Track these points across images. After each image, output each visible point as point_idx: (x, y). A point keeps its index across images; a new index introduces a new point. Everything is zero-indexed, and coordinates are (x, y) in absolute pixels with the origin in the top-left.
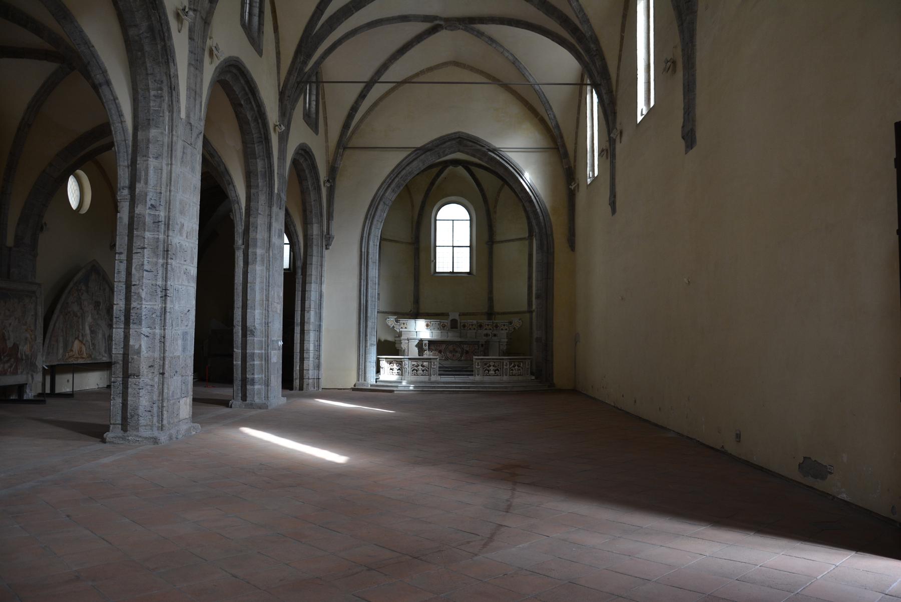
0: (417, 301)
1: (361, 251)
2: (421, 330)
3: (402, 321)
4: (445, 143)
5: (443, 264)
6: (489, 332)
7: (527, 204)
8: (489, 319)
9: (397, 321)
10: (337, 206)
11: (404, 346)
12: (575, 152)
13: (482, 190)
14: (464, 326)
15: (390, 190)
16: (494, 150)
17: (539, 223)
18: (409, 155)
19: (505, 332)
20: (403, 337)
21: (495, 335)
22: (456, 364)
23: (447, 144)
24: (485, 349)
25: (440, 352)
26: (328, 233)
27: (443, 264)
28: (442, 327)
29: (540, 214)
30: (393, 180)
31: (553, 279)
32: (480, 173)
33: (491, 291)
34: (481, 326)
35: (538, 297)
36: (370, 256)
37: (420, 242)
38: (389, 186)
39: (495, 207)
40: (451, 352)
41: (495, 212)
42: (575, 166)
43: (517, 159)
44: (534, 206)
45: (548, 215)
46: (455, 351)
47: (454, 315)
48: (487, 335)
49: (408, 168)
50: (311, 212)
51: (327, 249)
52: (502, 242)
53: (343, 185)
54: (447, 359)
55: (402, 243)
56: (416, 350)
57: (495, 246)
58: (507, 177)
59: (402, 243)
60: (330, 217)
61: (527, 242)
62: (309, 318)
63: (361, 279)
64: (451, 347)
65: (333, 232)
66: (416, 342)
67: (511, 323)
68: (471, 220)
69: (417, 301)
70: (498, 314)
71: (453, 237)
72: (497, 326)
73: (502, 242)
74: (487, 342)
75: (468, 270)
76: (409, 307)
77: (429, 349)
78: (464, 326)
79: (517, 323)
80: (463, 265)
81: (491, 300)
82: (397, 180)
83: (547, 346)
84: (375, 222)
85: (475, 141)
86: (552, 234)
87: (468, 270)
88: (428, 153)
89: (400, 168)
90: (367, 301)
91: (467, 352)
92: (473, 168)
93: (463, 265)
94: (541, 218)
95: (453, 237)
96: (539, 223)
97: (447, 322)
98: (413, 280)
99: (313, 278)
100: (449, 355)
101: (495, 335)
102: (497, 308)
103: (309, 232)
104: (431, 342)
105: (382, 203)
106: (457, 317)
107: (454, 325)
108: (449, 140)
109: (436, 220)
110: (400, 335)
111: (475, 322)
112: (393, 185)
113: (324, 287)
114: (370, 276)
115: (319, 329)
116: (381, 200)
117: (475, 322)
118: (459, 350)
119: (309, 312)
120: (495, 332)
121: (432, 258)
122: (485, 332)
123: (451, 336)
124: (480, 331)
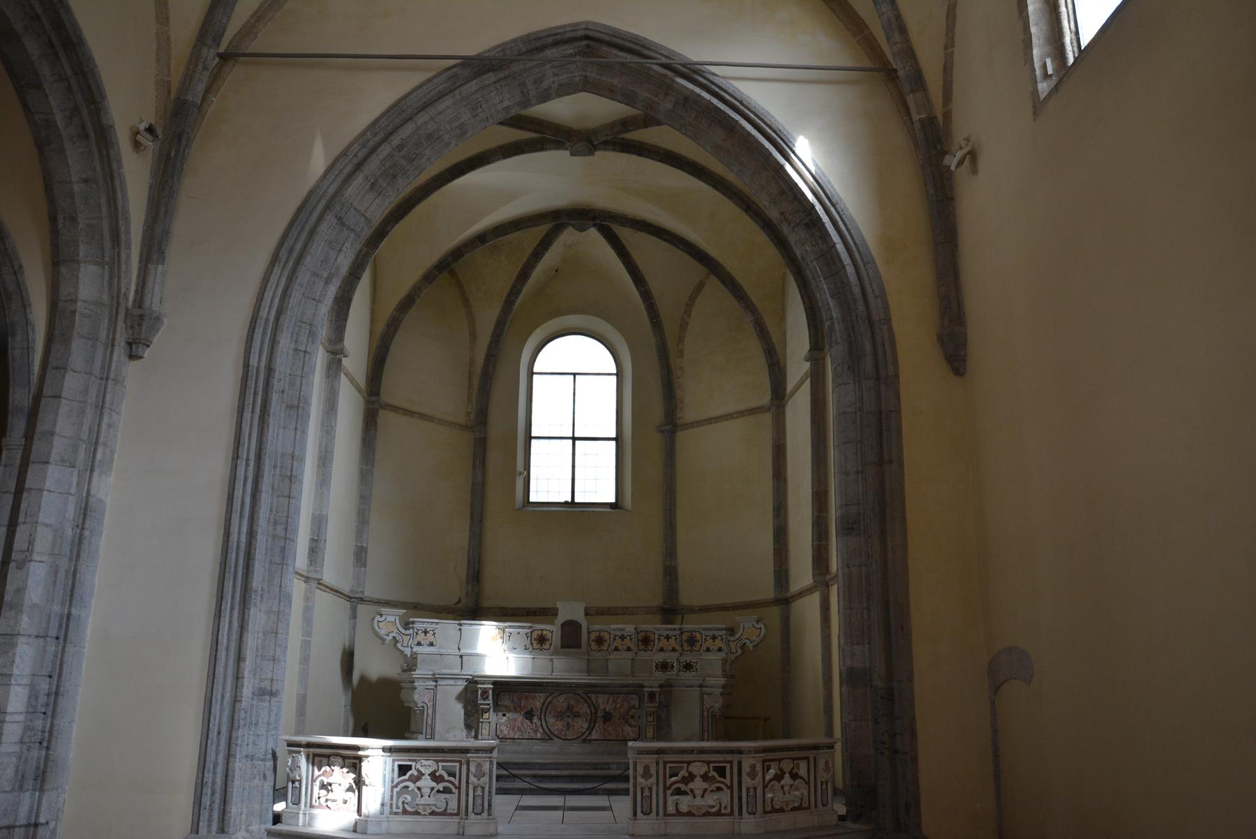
0: (475, 576)
1: (246, 366)
2: (496, 651)
3: (422, 623)
4: (541, 49)
5: (548, 480)
6: (671, 658)
7: (796, 237)
8: (667, 621)
9: (407, 625)
10: (183, 223)
11: (420, 697)
12: (947, 69)
13: (646, 295)
14: (600, 641)
15: (359, 179)
16: (692, 72)
17: (841, 291)
18: (429, 80)
19: (716, 657)
20: (418, 673)
21: (688, 667)
22: (575, 752)
23: (549, 53)
24: (657, 708)
25: (529, 715)
26: (139, 303)
27: (548, 480)
28: (539, 642)
29: (846, 259)
30: (373, 151)
31: (901, 465)
32: (643, 247)
33: (670, 551)
34: (646, 641)
35: (849, 527)
36: (277, 385)
37: (492, 428)
38: (359, 167)
39: (681, 339)
40: (560, 715)
41: (681, 353)
42: (947, 115)
43: (767, 99)
44: (825, 235)
45: (869, 261)
46: (571, 712)
47: (571, 611)
48: (664, 666)
49: (422, 118)
50: (73, 219)
51: (133, 357)
52: (699, 423)
53: (209, 162)
54: (548, 737)
55: (440, 422)
56: (459, 709)
57: (681, 436)
58: (742, 156)
59: (440, 422)
60: (154, 249)
61: (767, 418)
62: (20, 591)
63: (236, 457)
64: (561, 702)
65: (153, 301)
66: (461, 685)
67: (731, 631)
68: (619, 374)
69: (475, 576)
70: (691, 610)
71: (573, 416)
72: (692, 641)
73: (699, 423)
74: (667, 687)
75: (612, 499)
76: (454, 591)
77: (497, 707)
78: (600, 641)
79: (749, 628)
80: (598, 482)
81: (670, 573)
82: (385, 150)
83: (883, 693)
84: (303, 277)
85: (635, 47)
86: (888, 320)
87: (612, 499)
88: (490, 78)
89: (399, 114)
90: (252, 534)
91: (607, 717)
92: (625, 233)
93: (598, 482)
94: (850, 270)
95: (573, 416)
96: (841, 291)
97: (553, 630)
98: (475, 531)
99: (59, 447)
100: (557, 725)
101: (688, 667)
102: (688, 596)
103: (64, 291)
104: (503, 687)
105: (330, 218)
106: (580, 617)
107: (571, 637)
108: (556, 44)
109: (531, 373)
110: (410, 664)
111: (630, 628)
112: (373, 165)
113: (106, 488)
114: (269, 448)
115: (63, 631)
116: (328, 207)
117: (630, 628)
118: (585, 709)
119: (21, 565)
120: (688, 658)
121: (520, 466)
122: (660, 657)
123: (560, 669)
124: (643, 656)
